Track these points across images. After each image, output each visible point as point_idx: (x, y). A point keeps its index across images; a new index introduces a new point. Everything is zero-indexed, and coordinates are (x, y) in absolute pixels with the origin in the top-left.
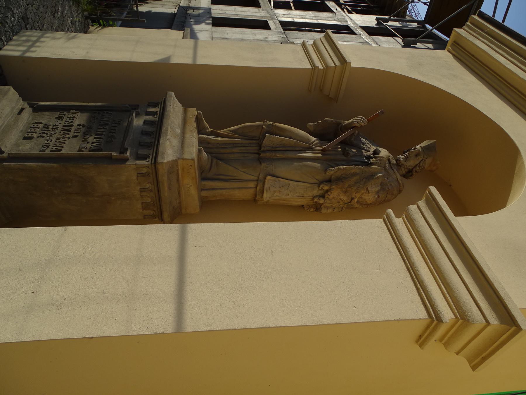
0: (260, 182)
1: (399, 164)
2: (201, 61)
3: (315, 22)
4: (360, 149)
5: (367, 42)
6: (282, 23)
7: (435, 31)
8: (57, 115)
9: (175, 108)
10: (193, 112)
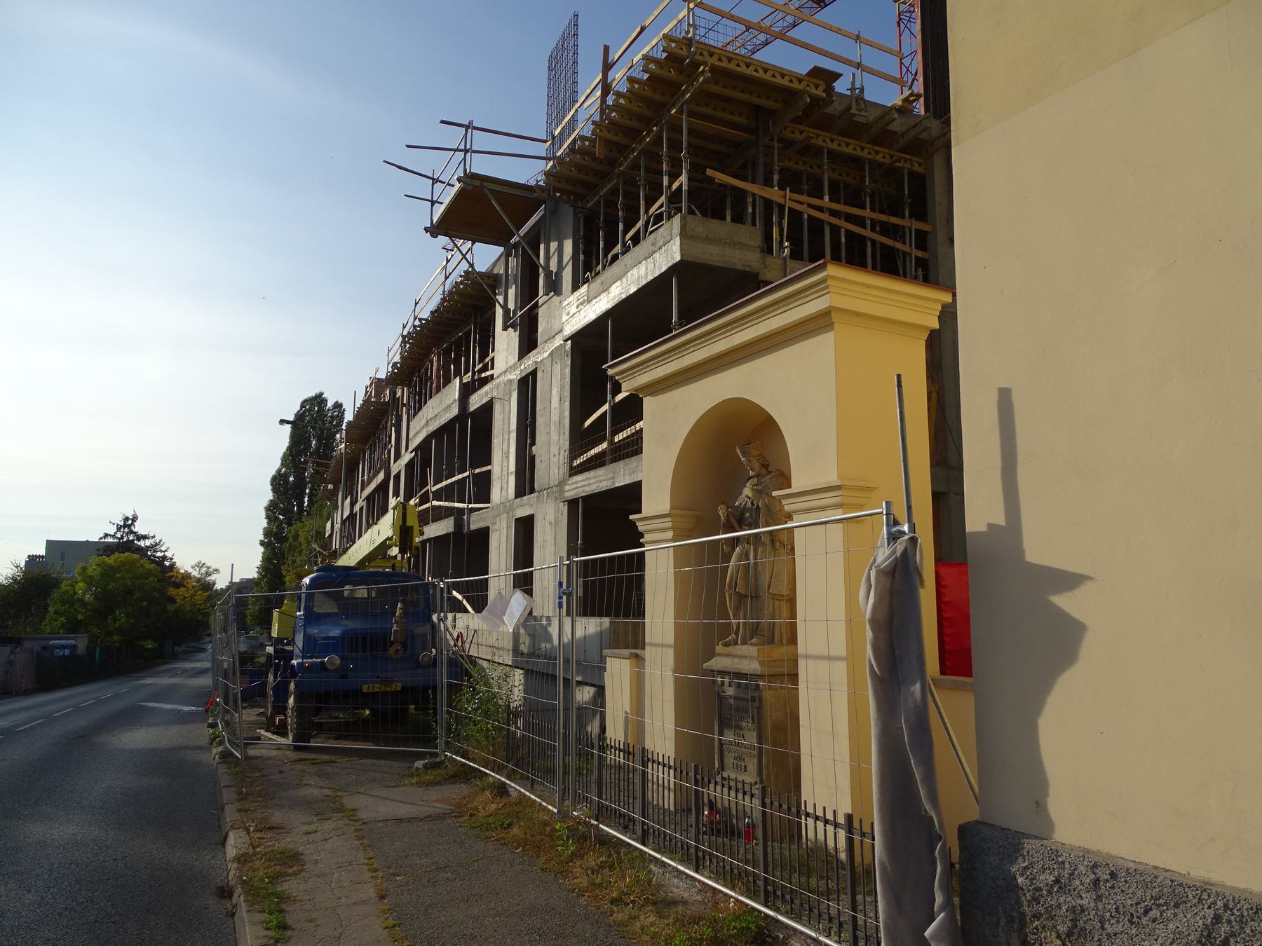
0: (774, 597)
1: (757, 476)
2: (670, 639)
3: (513, 436)
4: (745, 509)
5: (551, 354)
6: (520, 493)
7: (523, 232)
8: (726, 753)
9: (717, 663)
10: (719, 648)
